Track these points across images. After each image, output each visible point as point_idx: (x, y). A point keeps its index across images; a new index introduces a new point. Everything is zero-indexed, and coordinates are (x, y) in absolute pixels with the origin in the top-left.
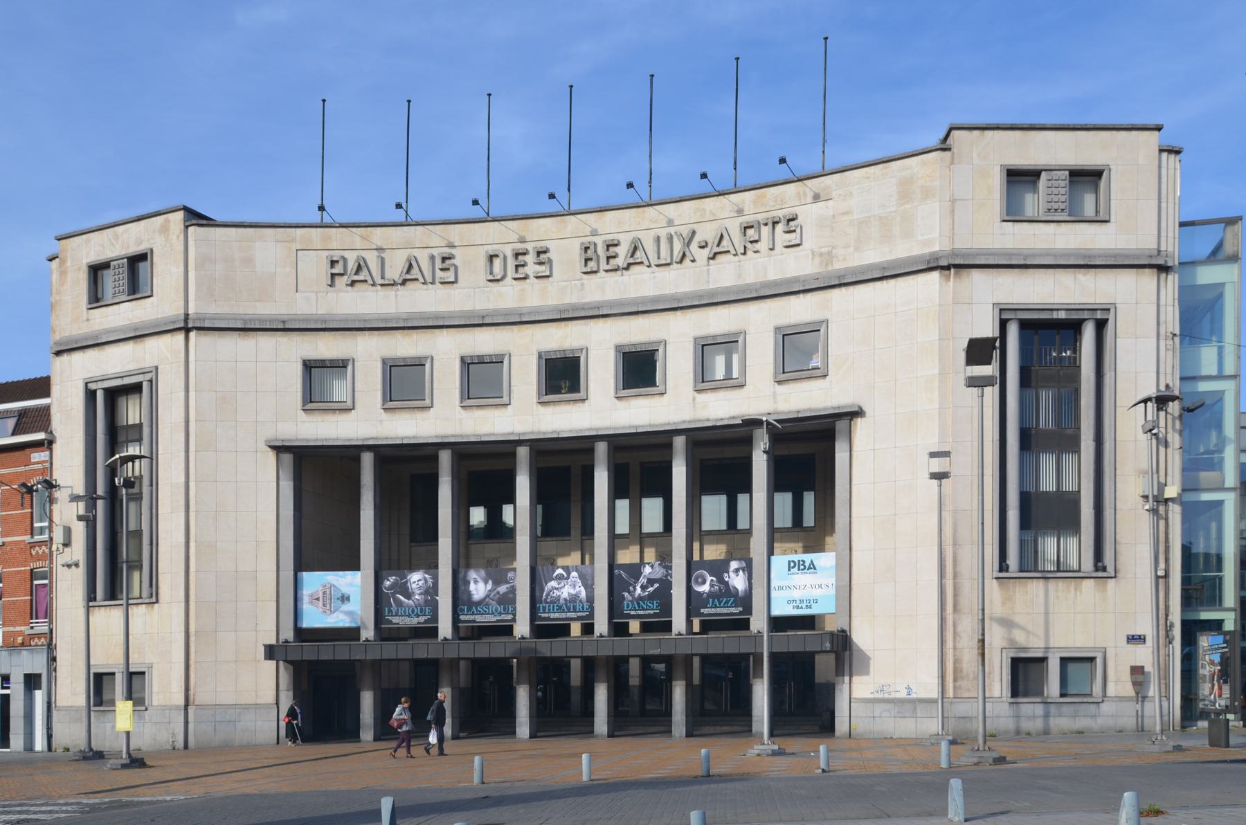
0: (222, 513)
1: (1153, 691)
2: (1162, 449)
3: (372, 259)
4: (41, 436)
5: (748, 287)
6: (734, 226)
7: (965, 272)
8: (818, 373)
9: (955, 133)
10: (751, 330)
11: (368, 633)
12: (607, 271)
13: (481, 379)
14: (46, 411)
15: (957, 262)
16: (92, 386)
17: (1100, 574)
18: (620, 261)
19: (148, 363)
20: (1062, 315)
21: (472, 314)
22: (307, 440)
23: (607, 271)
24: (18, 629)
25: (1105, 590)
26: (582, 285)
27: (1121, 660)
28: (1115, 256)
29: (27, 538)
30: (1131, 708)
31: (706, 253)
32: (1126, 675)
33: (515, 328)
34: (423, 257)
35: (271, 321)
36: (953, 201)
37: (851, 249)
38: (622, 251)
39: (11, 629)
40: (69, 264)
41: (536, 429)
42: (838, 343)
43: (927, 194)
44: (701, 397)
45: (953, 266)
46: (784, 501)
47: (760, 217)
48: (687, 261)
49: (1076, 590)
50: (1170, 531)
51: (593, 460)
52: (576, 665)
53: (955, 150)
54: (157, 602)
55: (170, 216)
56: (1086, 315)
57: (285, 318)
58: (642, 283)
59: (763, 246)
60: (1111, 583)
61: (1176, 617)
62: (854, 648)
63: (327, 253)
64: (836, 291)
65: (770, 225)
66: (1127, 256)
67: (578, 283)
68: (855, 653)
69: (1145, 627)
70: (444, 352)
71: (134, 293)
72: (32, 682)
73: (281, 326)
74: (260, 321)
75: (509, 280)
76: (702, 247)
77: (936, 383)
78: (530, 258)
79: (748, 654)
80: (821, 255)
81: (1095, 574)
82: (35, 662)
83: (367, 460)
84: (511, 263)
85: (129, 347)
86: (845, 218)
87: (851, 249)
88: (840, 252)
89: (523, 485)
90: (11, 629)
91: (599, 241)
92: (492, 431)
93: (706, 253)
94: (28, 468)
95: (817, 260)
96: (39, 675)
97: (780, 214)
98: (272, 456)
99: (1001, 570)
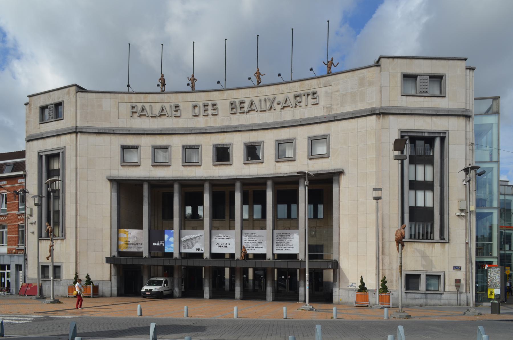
4: (21, 173)
6: (291, 96)
7: (386, 117)
10: (298, 137)
11: (146, 254)
12: (240, 113)
14: (23, 163)
15: (383, 112)
16: (41, 154)
17: (443, 241)
18: (246, 109)
19: (62, 145)
20: (426, 135)
21: (186, 129)
23: (240, 113)
24: (13, 247)
26: (230, 118)
27: (451, 277)
28: (448, 111)
29: (17, 212)
30: (454, 296)
31: (280, 106)
34: (167, 106)
35: (109, 130)
37: (339, 106)
38: (246, 105)
39: (11, 247)
40: (32, 106)
41: (212, 175)
43: (371, 84)
44: (278, 165)
47: (302, 92)
48: (272, 110)
49: (432, 247)
51: (266, 188)
52: (227, 270)
53: (382, 66)
55: (71, 88)
56: (436, 135)
57: (114, 129)
59: (303, 104)
60: (447, 245)
65: (306, 95)
66: (453, 111)
67: (229, 117)
69: (462, 263)
72: (19, 267)
73: (112, 132)
74: (105, 130)
75: (201, 116)
76: (278, 104)
78: (210, 107)
79: (296, 269)
80: (327, 108)
82: (20, 261)
83: (146, 187)
84: (202, 109)
86: (337, 93)
87: (339, 106)
88: (335, 107)
90: (11, 247)
91: (237, 101)
93: (280, 106)
94: (17, 185)
95: (325, 110)
97: (310, 91)
98: (108, 184)
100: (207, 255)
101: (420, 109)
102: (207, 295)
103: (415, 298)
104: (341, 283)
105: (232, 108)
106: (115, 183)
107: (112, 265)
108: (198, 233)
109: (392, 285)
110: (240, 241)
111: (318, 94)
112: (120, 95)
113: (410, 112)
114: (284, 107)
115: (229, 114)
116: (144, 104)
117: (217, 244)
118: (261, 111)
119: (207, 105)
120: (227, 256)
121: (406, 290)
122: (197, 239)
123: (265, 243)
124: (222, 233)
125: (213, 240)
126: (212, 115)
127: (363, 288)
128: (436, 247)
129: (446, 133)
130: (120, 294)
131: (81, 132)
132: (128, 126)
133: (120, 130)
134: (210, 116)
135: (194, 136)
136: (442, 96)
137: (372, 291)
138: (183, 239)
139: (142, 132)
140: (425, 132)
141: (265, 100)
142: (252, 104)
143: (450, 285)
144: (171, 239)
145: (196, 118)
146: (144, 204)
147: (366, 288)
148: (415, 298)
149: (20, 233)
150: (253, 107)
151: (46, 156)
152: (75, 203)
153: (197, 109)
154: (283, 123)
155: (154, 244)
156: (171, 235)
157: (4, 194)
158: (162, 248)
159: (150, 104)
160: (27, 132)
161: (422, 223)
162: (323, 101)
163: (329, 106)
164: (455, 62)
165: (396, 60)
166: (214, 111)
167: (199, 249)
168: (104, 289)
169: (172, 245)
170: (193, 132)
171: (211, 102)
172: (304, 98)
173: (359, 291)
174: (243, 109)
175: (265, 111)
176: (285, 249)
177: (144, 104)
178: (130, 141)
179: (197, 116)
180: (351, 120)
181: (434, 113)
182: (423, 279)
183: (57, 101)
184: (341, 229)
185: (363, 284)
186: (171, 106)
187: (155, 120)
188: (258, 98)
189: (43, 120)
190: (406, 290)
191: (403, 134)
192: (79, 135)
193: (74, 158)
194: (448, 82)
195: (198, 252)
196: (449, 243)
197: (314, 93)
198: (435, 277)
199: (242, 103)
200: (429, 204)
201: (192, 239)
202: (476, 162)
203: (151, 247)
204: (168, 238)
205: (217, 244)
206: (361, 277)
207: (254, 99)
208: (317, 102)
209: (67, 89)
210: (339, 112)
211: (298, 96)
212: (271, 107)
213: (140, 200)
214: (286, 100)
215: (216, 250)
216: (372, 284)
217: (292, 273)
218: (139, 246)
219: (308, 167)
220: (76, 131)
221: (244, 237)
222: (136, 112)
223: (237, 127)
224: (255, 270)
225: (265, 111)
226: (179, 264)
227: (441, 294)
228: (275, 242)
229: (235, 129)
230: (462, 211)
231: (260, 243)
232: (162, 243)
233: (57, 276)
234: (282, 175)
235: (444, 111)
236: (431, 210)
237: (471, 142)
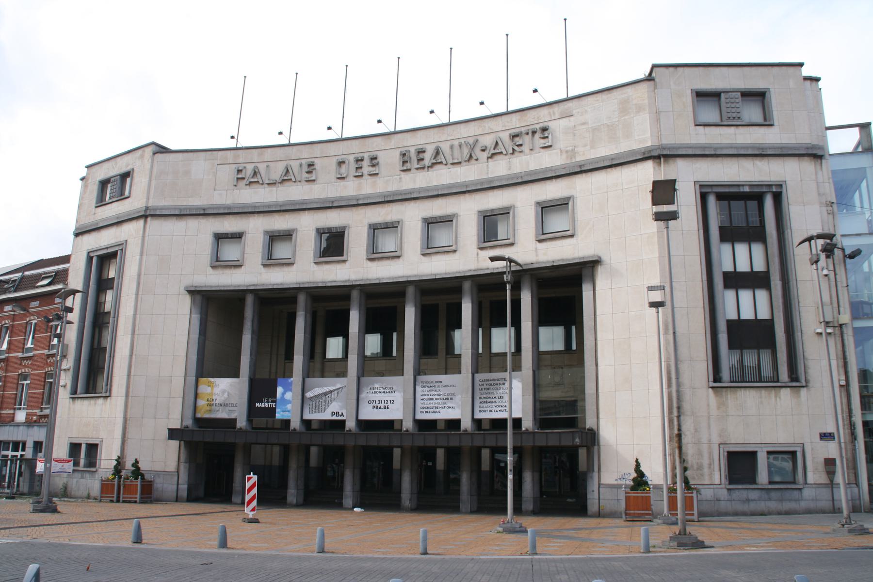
0: (156, 336)
1: (839, 478)
3: (262, 168)
6: (505, 136)
7: (671, 161)
9: (655, 69)
10: (518, 204)
11: (242, 423)
12: (417, 169)
13: (333, 244)
15: (665, 153)
16: (92, 254)
17: (794, 384)
19: (122, 239)
20: (747, 189)
21: (325, 200)
22: (211, 286)
23: (417, 169)
24: (34, 411)
25: (799, 396)
26: (400, 178)
27: (817, 452)
28: (781, 148)
29: (46, 352)
30: (825, 493)
31: (485, 155)
32: (821, 467)
33: (354, 209)
34: (295, 165)
35: (197, 209)
36: (658, 113)
37: (588, 147)
38: (428, 158)
39: (31, 411)
42: (582, 209)
43: (639, 109)
47: (523, 130)
48: (473, 161)
49: (776, 397)
50: (847, 350)
51: (296, 308)
52: (440, 453)
53: (657, 80)
56: (764, 189)
58: (442, 177)
60: (803, 391)
61: (858, 419)
62: (602, 442)
63: (400, 150)
65: (530, 134)
66: (791, 148)
67: (398, 177)
68: (602, 447)
71: (121, 195)
72: (38, 446)
73: (202, 212)
74: (190, 209)
75: (351, 178)
76: (483, 150)
77: (656, 239)
78: (366, 163)
80: (567, 152)
81: (790, 384)
83: (250, 300)
84: (353, 165)
86: (583, 127)
87: (588, 147)
88: (580, 149)
89: (410, 316)
90: (31, 411)
91: (413, 150)
92: (334, 279)
93: (485, 155)
95: (564, 156)
97: (538, 127)
98: (187, 299)
99: (715, 381)
100: (351, 424)
101: (731, 146)
103: (748, 500)
104: (602, 474)
105: (404, 162)
107: (182, 443)
108: (337, 383)
109: (702, 475)
110: (412, 396)
112: (220, 153)
113: (713, 153)
114: (493, 154)
115: (399, 172)
116: (258, 165)
117: (370, 402)
118: (452, 164)
119: (362, 160)
121: (730, 483)
122: (334, 394)
123: (458, 398)
124: (379, 383)
125: (362, 396)
126: (370, 175)
127: (640, 481)
128: (782, 397)
129: (781, 185)
130: (192, 497)
133: (214, 208)
134: (366, 177)
135: (338, 211)
136: (767, 122)
137: (658, 488)
138: (309, 395)
139: (250, 210)
140: (743, 185)
142: (437, 152)
143: (815, 471)
144: (289, 396)
145: (342, 183)
146: (244, 333)
147: (646, 483)
148: (748, 500)
149: (47, 387)
150: (441, 158)
151: (98, 256)
152: (130, 333)
153: (344, 166)
154: (490, 180)
155: (257, 405)
156: (287, 388)
157: (34, 322)
158: (272, 411)
159: (267, 164)
161: (751, 350)
163: (570, 148)
164: (784, 68)
165: (681, 69)
166: (373, 169)
167: (337, 414)
168: (165, 486)
169: (289, 407)
170: (335, 204)
171: (368, 154)
172: (527, 139)
173: (633, 488)
174: (422, 163)
175: (460, 163)
176: (496, 409)
177: (258, 165)
178: (229, 225)
179: (343, 178)
181: (757, 153)
183: (124, 170)
184: (599, 368)
185: (640, 474)
186: (301, 165)
187: (274, 189)
188: (448, 144)
189: (101, 201)
190: (730, 483)
191: (704, 190)
192: (149, 219)
193: (138, 257)
194: (775, 100)
195: (335, 418)
196: (806, 386)
197: (544, 130)
199: (421, 152)
200: (764, 314)
201: (325, 394)
203: (252, 412)
204: (283, 394)
205: (370, 402)
206: (637, 461)
207: (441, 145)
208: (550, 144)
209: (140, 152)
211: (516, 136)
212: (471, 157)
213: (246, 326)
214: (497, 143)
215: (368, 413)
216: (656, 473)
218: (231, 408)
219: (537, 256)
220: (146, 215)
221: (419, 389)
222: (243, 178)
225: (460, 163)
227: (800, 489)
228: (477, 396)
229: (409, 196)
230: (827, 324)
231: (448, 399)
232: (273, 402)
233: (92, 461)
234: (489, 272)
235: (775, 148)
236: (768, 326)
237: (829, 199)
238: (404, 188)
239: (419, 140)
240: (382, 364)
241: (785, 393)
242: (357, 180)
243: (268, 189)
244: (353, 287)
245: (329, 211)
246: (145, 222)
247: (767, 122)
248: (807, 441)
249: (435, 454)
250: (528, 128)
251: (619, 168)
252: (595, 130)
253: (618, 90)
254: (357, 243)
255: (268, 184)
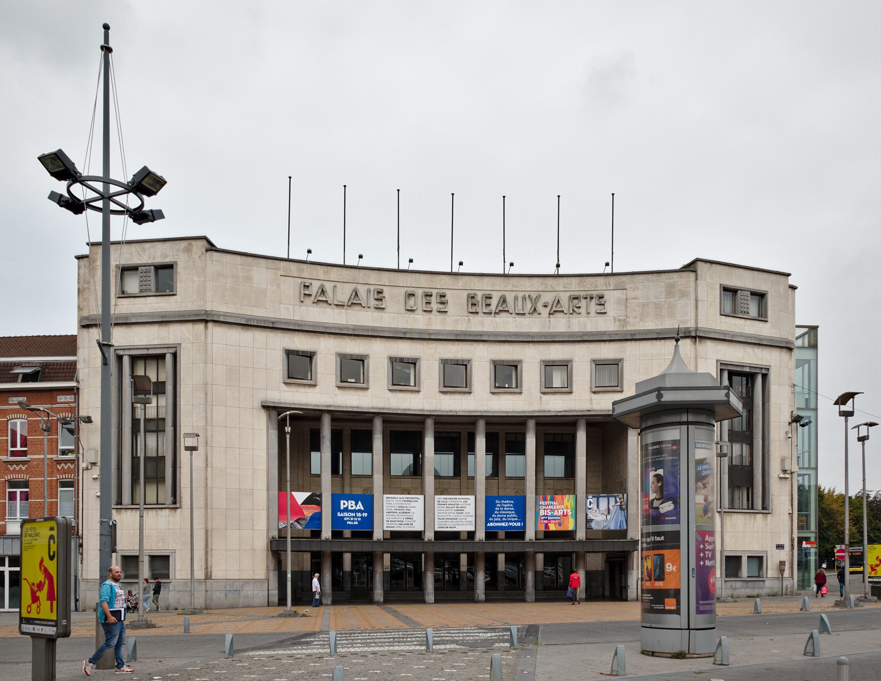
1: (787, 574)
2: (855, 446)
3: (328, 287)
5: (574, 334)
6: (564, 298)
7: (703, 341)
8: (618, 389)
9: (699, 263)
13: (403, 372)
14: (73, 364)
15: (701, 335)
16: (121, 353)
18: (493, 308)
20: (747, 370)
21: (396, 330)
27: (773, 558)
33: (425, 343)
34: (362, 290)
37: (638, 320)
38: (494, 302)
41: (438, 408)
43: (684, 294)
44: (545, 397)
45: (205, 319)
46: (448, 459)
47: (582, 293)
51: (525, 430)
52: (464, 558)
54: (180, 508)
57: (273, 320)
58: (507, 324)
59: (583, 310)
60: (769, 516)
63: (468, 292)
64: (629, 344)
70: (378, 354)
73: (271, 325)
74: (258, 321)
75: (420, 311)
76: (546, 306)
79: (420, 554)
80: (620, 320)
85: (155, 329)
88: (631, 320)
89: (481, 443)
91: (479, 294)
94: (54, 406)
95: (617, 323)
96: (868, 544)
97: (594, 293)
98: (263, 416)
102: (430, 596)
103: (735, 589)
106: (274, 413)
111: (606, 298)
118: (517, 314)
119: (431, 296)
120: (464, 536)
131: (214, 321)
132: (297, 318)
139: (321, 330)
141: (524, 298)
145: (412, 316)
153: (412, 299)
159: (333, 284)
160: (80, 308)
162: (611, 307)
166: (442, 306)
170: (408, 336)
171: (483, 292)
172: (583, 303)
177: (325, 283)
180: (654, 342)
182: (744, 560)
188: (514, 294)
197: (601, 297)
198: (758, 560)
202: (798, 409)
207: (507, 294)
209: (184, 244)
210: (637, 328)
217: (415, 558)
222: (310, 295)
223: (481, 334)
224: (394, 555)
226: (431, 550)
229: (479, 338)
234: (554, 414)
238: (473, 329)
239: (486, 285)
240: (407, 483)
241: (759, 516)
242: (427, 315)
243: (337, 310)
244: (322, 411)
245: (400, 341)
246: (206, 327)
247: (762, 317)
248: (769, 549)
249: (459, 558)
250: (589, 290)
251: (663, 342)
252: (644, 306)
253: (666, 275)
254: (531, 376)
255: (337, 305)
